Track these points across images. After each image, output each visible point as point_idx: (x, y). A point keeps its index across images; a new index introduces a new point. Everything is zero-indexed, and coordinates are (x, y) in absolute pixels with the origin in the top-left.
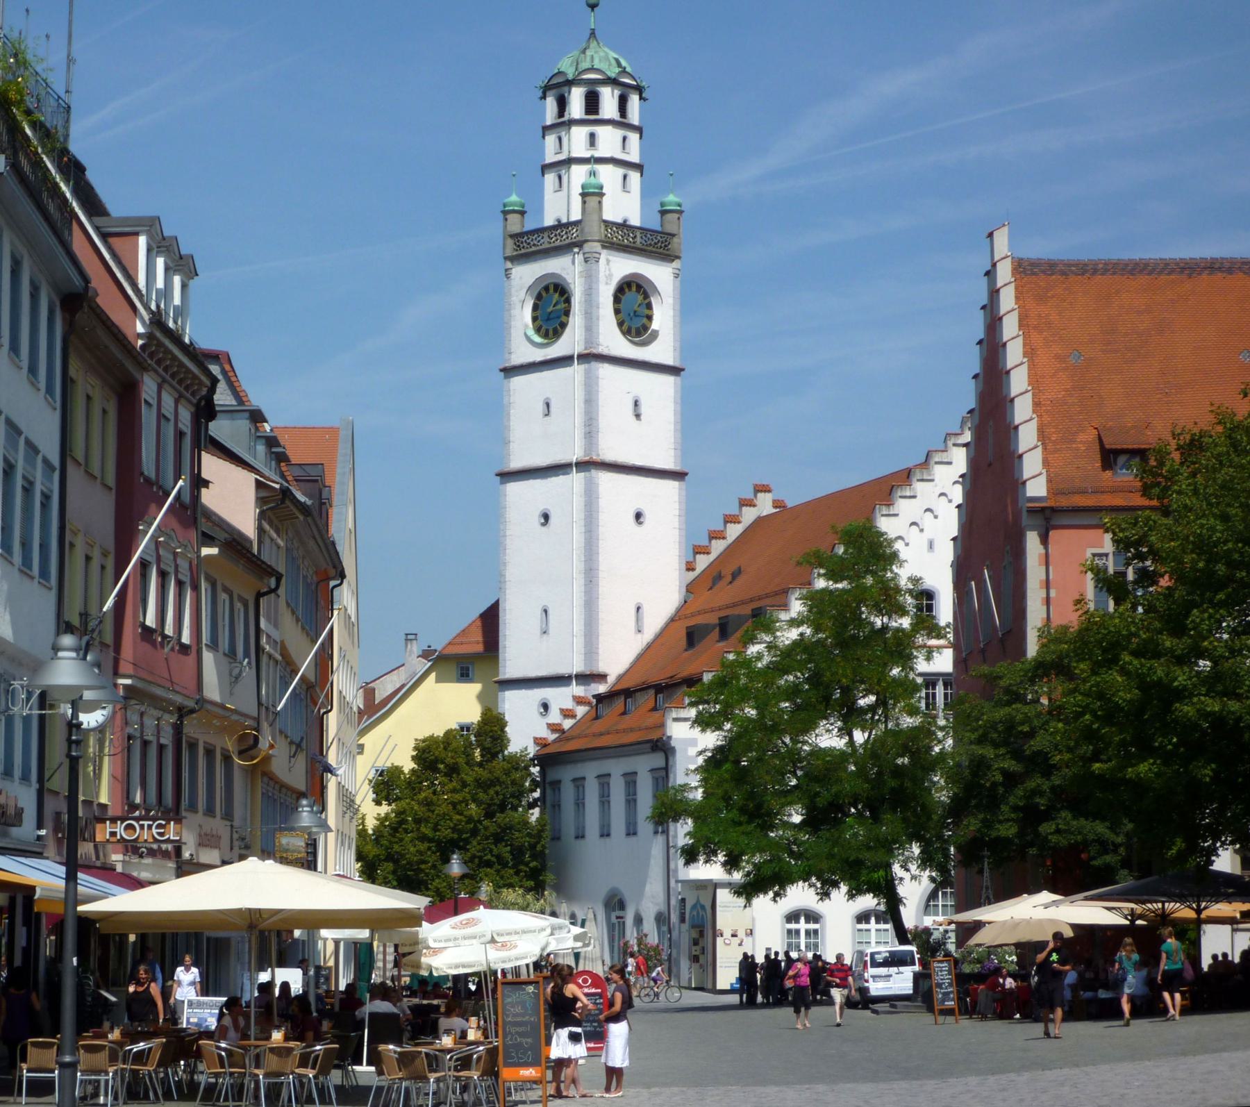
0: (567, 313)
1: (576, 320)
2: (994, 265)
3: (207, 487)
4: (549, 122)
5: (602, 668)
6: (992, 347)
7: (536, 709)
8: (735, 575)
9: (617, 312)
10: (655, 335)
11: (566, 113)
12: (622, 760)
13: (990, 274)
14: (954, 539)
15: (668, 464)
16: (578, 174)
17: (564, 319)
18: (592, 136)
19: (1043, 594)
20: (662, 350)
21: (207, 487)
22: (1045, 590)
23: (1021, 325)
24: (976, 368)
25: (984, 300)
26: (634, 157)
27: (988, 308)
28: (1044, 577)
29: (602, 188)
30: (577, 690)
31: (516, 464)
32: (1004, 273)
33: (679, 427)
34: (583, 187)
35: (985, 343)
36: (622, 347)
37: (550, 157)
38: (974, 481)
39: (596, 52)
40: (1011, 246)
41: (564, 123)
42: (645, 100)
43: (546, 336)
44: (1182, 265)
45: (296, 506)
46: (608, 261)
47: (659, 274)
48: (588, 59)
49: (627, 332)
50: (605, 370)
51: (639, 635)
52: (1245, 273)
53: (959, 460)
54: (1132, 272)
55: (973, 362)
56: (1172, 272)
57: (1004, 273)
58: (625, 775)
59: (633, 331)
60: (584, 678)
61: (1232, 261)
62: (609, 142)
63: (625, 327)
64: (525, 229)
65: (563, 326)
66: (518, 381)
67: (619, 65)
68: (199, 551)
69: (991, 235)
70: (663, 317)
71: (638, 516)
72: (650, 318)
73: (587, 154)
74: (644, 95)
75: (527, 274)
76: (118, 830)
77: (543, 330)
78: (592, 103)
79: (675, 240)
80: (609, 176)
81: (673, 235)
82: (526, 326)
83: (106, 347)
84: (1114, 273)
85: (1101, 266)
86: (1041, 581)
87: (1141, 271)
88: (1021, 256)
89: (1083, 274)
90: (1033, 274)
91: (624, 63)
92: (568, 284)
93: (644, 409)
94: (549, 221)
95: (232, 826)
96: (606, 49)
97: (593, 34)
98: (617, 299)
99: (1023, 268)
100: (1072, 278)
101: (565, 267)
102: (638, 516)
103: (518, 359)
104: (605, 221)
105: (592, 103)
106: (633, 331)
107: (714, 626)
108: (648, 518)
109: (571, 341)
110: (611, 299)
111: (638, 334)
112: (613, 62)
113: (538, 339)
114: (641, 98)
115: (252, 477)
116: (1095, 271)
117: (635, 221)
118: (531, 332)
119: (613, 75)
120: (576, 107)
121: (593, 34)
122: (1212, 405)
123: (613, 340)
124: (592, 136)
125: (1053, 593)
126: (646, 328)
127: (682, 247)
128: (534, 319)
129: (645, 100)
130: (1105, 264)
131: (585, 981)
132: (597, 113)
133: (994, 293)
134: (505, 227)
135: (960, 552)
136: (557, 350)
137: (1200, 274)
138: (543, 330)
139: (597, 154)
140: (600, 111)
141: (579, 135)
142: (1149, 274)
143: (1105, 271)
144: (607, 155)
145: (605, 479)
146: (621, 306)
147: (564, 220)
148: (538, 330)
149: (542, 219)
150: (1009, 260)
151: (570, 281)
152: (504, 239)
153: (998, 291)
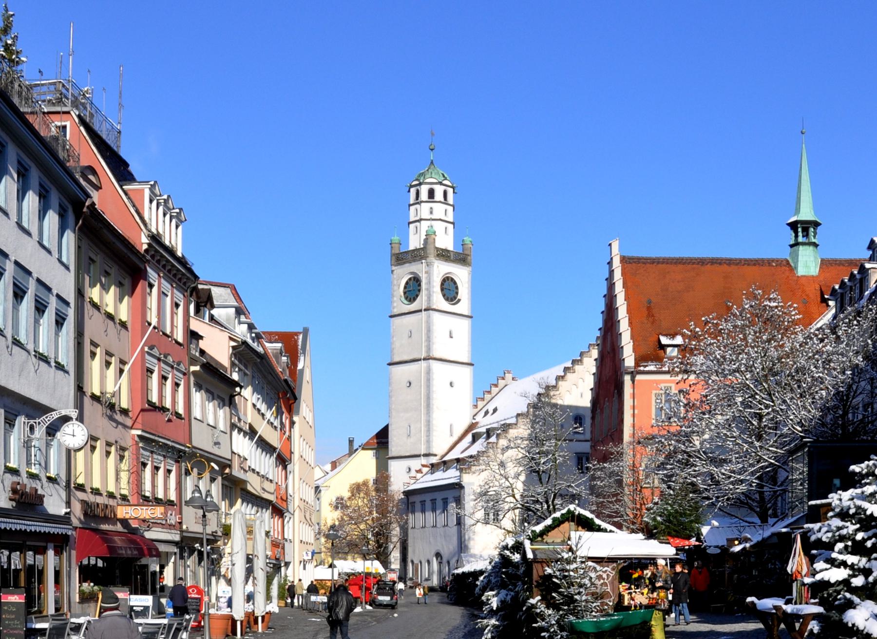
0: (419, 291)
1: (424, 293)
2: (612, 259)
3: (202, 339)
4: (411, 202)
5: (434, 451)
6: (610, 298)
7: (406, 470)
8: (495, 410)
9: (442, 290)
10: (459, 300)
11: (419, 199)
12: (441, 492)
13: (610, 263)
14: (592, 389)
15: (466, 360)
16: (424, 225)
17: (418, 293)
18: (431, 213)
19: (632, 412)
20: (464, 306)
21: (202, 339)
22: (632, 410)
23: (622, 274)
24: (603, 308)
25: (607, 276)
26: (450, 218)
27: (609, 280)
28: (632, 404)
29: (435, 232)
30: (424, 461)
31: (397, 359)
32: (617, 263)
33: (470, 343)
34: (427, 231)
35: (607, 296)
36: (445, 305)
37: (412, 219)
38: (601, 362)
39: (433, 170)
40: (620, 249)
41: (418, 201)
42: (456, 193)
43: (410, 301)
44: (699, 261)
45: (252, 351)
46: (438, 266)
47: (462, 275)
48: (430, 173)
49: (447, 299)
50: (436, 316)
51: (452, 437)
52: (727, 265)
53: (595, 353)
54: (676, 263)
55: (602, 306)
56: (694, 263)
57: (617, 263)
58: (443, 499)
59: (449, 299)
60: (427, 455)
61: (722, 259)
62: (439, 210)
63: (446, 297)
64: (402, 251)
65: (417, 296)
66: (397, 320)
67: (444, 176)
68: (189, 368)
69: (610, 245)
70: (464, 292)
71: (451, 384)
72: (457, 293)
73: (428, 217)
74: (455, 191)
75: (402, 275)
76: (129, 512)
77: (408, 299)
78: (431, 193)
79: (469, 258)
80: (439, 227)
81: (468, 255)
82: (401, 296)
83: (114, 243)
84: (667, 263)
85: (661, 260)
86: (631, 406)
87: (680, 263)
88: (624, 255)
89: (653, 264)
90: (630, 263)
91: (446, 176)
92: (420, 277)
93: (453, 335)
94: (411, 248)
95: (218, 514)
96: (438, 169)
97: (432, 162)
98: (442, 284)
99: (624, 260)
100: (648, 265)
101: (419, 268)
102: (451, 384)
103: (396, 311)
104: (437, 248)
105: (431, 193)
106: (449, 299)
107: (484, 433)
108: (455, 384)
109: (421, 302)
110: (440, 284)
111: (452, 300)
112: (441, 175)
113: (406, 302)
114: (454, 192)
115: (226, 335)
116: (658, 263)
117: (451, 248)
118: (403, 299)
119: (440, 181)
120: (424, 196)
121: (432, 162)
122: (693, 391)
123: (439, 301)
124: (431, 213)
125: (636, 412)
126: (455, 298)
127: (472, 261)
128: (405, 293)
129: (456, 193)
130: (664, 259)
131: (193, 591)
132: (433, 198)
133: (611, 272)
134: (391, 251)
135: (594, 396)
136: (414, 306)
137: (707, 264)
138: (408, 299)
139: (433, 218)
140: (435, 198)
141: (425, 207)
142: (683, 264)
143: (663, 263)
144: (438, 218)
145: (434, 365)
146: (444, 287)
147: (418, 247)
148: (406, 298)
149: (408, 245)
150: (619, 256)
151: (420, 275)
152: (391, 257)
153: (613, 271)
